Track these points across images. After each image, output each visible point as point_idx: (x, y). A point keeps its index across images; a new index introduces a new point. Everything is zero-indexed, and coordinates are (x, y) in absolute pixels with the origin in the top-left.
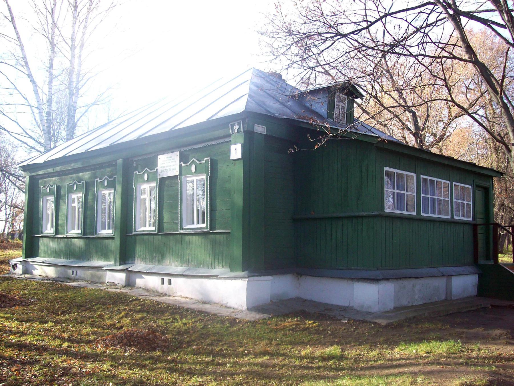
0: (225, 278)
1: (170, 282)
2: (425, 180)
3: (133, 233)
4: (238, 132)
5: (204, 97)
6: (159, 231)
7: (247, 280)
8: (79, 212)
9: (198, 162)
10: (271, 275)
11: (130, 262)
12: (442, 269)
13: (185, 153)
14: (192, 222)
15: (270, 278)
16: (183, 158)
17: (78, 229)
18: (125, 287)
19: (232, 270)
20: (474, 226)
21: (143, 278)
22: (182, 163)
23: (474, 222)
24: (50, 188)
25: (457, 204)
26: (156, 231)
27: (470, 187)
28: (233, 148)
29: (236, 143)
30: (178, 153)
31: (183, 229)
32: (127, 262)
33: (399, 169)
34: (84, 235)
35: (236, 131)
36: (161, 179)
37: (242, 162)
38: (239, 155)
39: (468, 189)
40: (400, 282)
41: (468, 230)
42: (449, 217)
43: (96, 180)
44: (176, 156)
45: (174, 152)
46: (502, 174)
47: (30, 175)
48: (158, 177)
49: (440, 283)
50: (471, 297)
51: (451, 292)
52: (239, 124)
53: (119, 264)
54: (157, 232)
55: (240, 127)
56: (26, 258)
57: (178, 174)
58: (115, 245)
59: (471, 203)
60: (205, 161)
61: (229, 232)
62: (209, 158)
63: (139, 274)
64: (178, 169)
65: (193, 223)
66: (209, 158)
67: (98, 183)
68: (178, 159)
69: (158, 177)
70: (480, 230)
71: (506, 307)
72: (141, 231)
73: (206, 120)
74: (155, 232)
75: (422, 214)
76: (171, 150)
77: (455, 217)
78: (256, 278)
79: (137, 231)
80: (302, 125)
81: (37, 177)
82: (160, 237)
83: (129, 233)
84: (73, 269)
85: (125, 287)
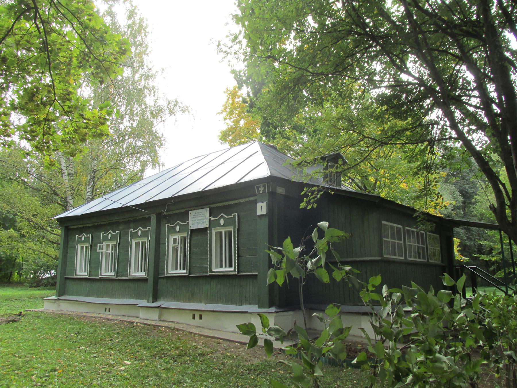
1: (201, 317)
2: (408, 231)
3: (166, 275)
5: (222, 164)
6: (190, 274)
8: (181, 256)
10: (292, 311)
11: (162, 299)
14: (174, 268)
15: (291, 313)
17: (85, 271)
19: (259, 307)
26: (76, 275)
27: (438, 236)
28: (259, 205)
29: (262, 201)
30: (208, 209)
31: (212, 272)
33: (391, 222)
35: (261, 192)
38: (264, 212)
42: (403, 258)
45: (203, 208)
48: (190, 229)
52: (264, 186)
54: (188, 274)
55: (265, 189)
57: (208, 226)
61: (256, 275)
62: (236, 214)
64: (208, 223)
65: (221, 267)
66: (236, 214)
68: (207, 214)
69: (190, 229)
72: (217, 272)
73: (235, 183)
74: (234, 273)
75: (430, 261)
76: (201, 206)
77: (430, 261)
78: (286, 313)
79: (214, 272)
84: (106, 306)
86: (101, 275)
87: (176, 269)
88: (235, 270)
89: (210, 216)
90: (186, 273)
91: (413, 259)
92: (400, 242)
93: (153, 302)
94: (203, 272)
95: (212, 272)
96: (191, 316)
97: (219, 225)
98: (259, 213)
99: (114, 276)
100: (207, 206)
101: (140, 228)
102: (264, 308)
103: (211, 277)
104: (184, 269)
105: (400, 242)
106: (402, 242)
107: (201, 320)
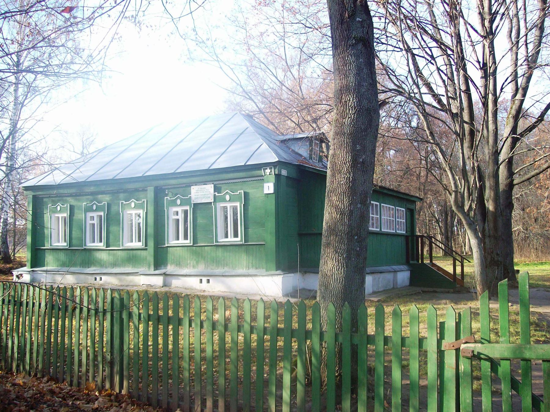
0: (263, 276)
1: (208, 281)
2: (398, 210)
3: (166, 245)
4: (270, 174)
6: (194, 244)
7: (282, 276)
9: (232, 194)
10: (293, 273)
11: (162, 268)
12: (394, 267)
13: (217, 185)
15: (292, 275)
16: (217, 189)
18: (162, 287)
19: (267, 271)
20: (406, 237)
21: (180, 279)
22: (216, 193)
23: (407, 234)
24: (61, 207)
25: (398, 221)
27: (404, 209)
29: (268, 182)
31: (218, 242)
32: (160, 268)
34: (107, 247)
35: (268, 174)
36: (194, 204)
37: (274, 195)
38: (271, 191)
39: (403, 211)
40: (373, 275)
41: (403, 239)
42: (379, 230)
43: (121, 202)
44: (210, 188)
46: (421, 199)
47: (33, 194)
48: (192, 202)
49: (390, 276)
50: (404, 287)
51: (397, 283)
53: (153, 270)
54: (192, 244)
56: (31, 268)
57: (213, 201)
58: (149, 255)
59: (405, 221)
60: (238, 193)
63: (176, 277)
67: (123, 205)
68: (212, 190)
69: (192, 202)
70: (410, 239)
71: (431, 291)
74: (242, 243)
77: (397, 231)
79: (220, 242)
80: (307, 169)
81: (40, 196)
82: (194, 248)
83: (39, 247)
84: (95, 276)
85: (162, 287)
86: (85, 245)
87: (132, 241)
88: (241, 240)
89: (215, 191)
90: (67, 246)
91: (374, 229)
92: (377, 216)
93: (154, 270)
94: (211, 243)
95: (218, 242)
96: (199, 281)
97: (224, 200)
98: (266, 191)
99: (67, 246)
100: (212, 183)
101: (133, 200)
102: (271, 270)
103: (85, 249)
104: (139, 241)
105: (377, 216)
106: (379, 217)
107: (201, 284)
